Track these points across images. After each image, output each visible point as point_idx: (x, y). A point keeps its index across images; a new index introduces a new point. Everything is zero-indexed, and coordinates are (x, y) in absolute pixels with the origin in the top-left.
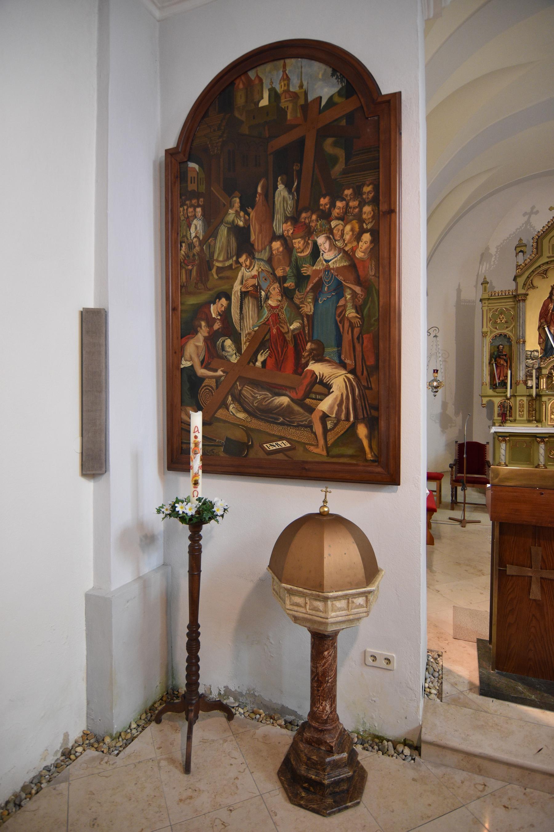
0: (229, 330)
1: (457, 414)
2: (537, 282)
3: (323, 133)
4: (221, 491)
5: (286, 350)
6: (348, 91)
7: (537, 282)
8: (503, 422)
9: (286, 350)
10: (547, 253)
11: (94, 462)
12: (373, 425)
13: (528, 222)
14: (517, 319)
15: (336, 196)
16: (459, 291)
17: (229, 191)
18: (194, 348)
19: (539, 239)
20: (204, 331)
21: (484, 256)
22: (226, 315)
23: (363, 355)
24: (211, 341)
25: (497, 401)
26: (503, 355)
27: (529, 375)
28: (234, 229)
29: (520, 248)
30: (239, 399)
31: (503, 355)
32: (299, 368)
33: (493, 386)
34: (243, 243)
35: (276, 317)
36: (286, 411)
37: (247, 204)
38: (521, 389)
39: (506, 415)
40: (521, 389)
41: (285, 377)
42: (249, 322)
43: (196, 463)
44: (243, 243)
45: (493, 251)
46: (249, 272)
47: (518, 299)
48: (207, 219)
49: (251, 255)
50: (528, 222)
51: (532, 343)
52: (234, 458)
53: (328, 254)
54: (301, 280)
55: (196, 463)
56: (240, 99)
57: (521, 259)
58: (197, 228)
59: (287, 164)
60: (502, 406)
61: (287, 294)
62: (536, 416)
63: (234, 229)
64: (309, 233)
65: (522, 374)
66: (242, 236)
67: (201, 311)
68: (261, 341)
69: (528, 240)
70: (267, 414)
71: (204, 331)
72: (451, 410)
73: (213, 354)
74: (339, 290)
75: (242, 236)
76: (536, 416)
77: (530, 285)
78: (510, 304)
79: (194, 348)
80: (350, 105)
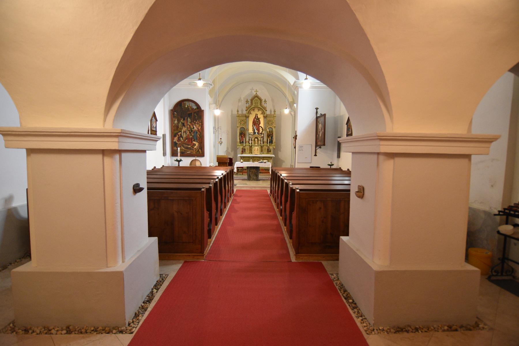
0: (181, 136)
1: (232, 151)
2: (252, 112)
3: (195, 113)
4: (182, 158)
5: (190, 140)
6: (198, 108)
7: (252, 112)
8: (242, 153)
9: (190, 140)
10: (254, 105)
11: (164, 154)
12: (201, 149)
13: (251, 92)
14: (246, 123)
15: (196, 121)
16: (232, 111)
17: (181, 117)
18: (176, 139)
19: (252, 100)
20: (177, 136)
21: (240, 100)
22: (181, 134)
23: (188, 262)
24: (179, 138)
25: (241, 147)
26: (243, 134)
27: (249, 140)
28: (182, 123)
29: (247, 102)
30: (183, 146)
31: (243, 134)
32: (192, 142)
33: (240, 143)
34: (183, 125)
35: (188, 135)
36: (190, 148)
37: (184, 120)
38: (247, 144)
39: (243, 151)
40: (247, 144)
41: (190, 143)
42: (184, 136)
43: (179, 154)
44: (183, 125)
45: (242, 99)
46: (184, 129)
47: (247, 117)
48: (178, 121)
49: (184, 126)
50: (251, 92)
51: (251, 130)
52: (183, 154)
53: (195, 128)
54: (192, 131)
55: (179, 154)
56: (183, 105)
57: (247, 105)
58: (176, 122)
59: (190, 115)
60: (243, 149)
61: (190, 132)
62: (251, 152)
63: (182, 123)
64: (193, 125)
65: (247, 140)
66: (183, 124)
67: (177, 134)
68: (186, 138)
69: (249, 99)
70: (187, 148)
71: (177, 136)
72: (230, 150)
73: (179, 140)
74: (197, 133)
75: (183, 124)
76: (251, 152)
77: (249, 113)
78: (244, 118)
79: (176, 139)
80: (198, 110)
